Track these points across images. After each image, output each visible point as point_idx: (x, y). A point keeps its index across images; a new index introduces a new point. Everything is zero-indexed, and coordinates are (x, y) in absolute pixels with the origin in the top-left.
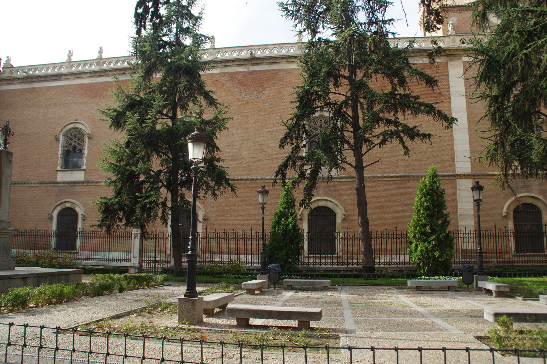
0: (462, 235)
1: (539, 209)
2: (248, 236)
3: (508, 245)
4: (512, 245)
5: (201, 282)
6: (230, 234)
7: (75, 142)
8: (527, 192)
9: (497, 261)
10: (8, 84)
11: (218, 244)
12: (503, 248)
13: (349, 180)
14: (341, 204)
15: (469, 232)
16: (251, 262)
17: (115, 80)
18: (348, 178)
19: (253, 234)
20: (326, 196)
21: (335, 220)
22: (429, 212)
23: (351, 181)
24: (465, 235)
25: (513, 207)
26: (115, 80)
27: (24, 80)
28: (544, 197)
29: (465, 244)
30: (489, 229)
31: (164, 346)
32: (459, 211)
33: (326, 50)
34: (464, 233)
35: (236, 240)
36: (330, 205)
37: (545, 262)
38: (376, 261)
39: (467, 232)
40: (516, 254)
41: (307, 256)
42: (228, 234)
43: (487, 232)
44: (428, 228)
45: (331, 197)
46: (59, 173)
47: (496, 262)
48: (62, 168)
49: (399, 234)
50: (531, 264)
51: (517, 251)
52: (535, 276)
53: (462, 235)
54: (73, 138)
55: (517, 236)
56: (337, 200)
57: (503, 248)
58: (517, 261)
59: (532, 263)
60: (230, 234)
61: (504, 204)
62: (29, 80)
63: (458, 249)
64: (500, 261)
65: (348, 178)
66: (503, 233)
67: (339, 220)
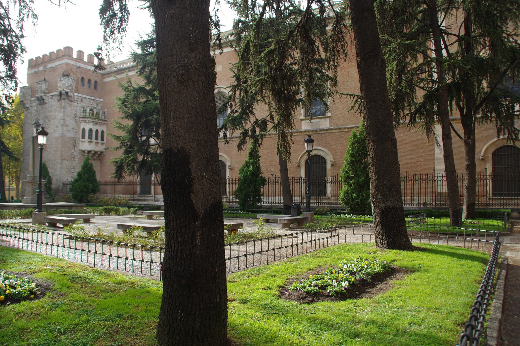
0: (403, 178)
2: (431, 178)
3: (485, 189)
4: (489, 188)
5: (228, 217)
6: (422, 176)
7: (220, 104)
9: (436, 204)
10: (109, 77)
11: (406, 187)
12: (480, 191)
13: (337, 131)
14: (331, 153)
15: (410, 176)
16: (272, 202)
17: (115, 78)
18: (336, 129)
20: (319, 146)
21: (326, 166)
22: (353, 159)
23: (339, 132)
24: (405, 178)
25: (492, 150)
26: (115, 78)
27: (117, 73)
29: (441, 187)
30: (429, 173)
31: (89, 258)
32: (436, 156)
33: (282, 35)
34: (405, 176)
35: (415, 181)
36: (321, 154)
37: (518, 205)
38: (312, 202)
39: (408, 176)
40: (494, 197)
41: (491, 197)
42: (419, 176)
43: (426, 176)
44: (351, 173)
45: (323, 146)
46: (303, 122)
47: (434, 204)
48: (305, 117)
49: (478, 176)
50: (333, 205)
51: (494, 194)
52: (436, 216)
53: (403, 178)
54: (218, 101)
55: (495, 178)
56: (327, 149)
57: (480, 191)
58: (492, 204)
59: (334, 204)
60: (422, 176)
61: (483, 147)
62: (120, 72)
63: (434, 192)
64: (438, 204)
65: (336, 129)
66: (483, 176)
67: (329, 166)
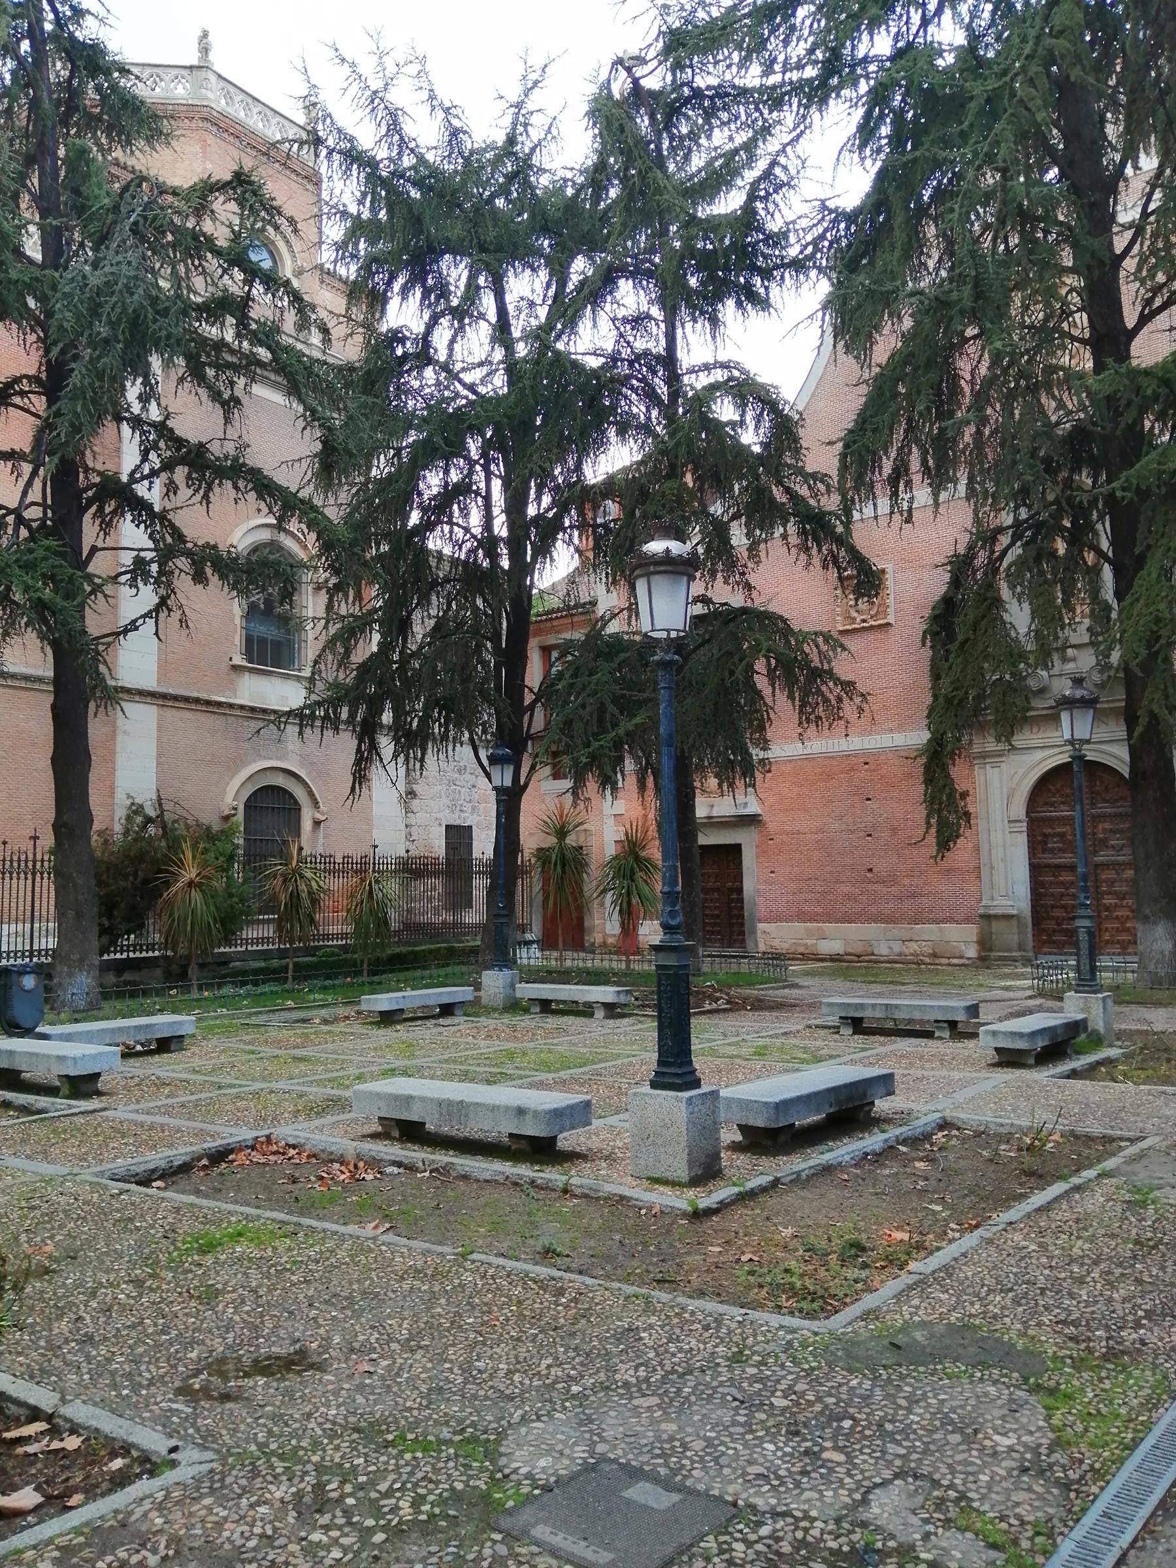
1: (296, 802)
8: (279, 759)
19: (39, 857)
28: (308, 774)
